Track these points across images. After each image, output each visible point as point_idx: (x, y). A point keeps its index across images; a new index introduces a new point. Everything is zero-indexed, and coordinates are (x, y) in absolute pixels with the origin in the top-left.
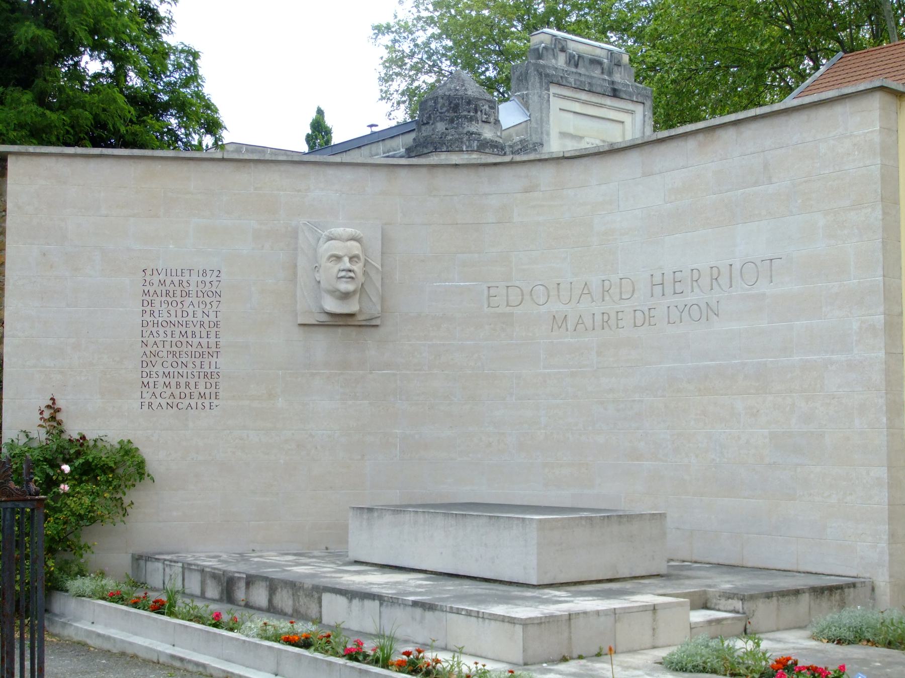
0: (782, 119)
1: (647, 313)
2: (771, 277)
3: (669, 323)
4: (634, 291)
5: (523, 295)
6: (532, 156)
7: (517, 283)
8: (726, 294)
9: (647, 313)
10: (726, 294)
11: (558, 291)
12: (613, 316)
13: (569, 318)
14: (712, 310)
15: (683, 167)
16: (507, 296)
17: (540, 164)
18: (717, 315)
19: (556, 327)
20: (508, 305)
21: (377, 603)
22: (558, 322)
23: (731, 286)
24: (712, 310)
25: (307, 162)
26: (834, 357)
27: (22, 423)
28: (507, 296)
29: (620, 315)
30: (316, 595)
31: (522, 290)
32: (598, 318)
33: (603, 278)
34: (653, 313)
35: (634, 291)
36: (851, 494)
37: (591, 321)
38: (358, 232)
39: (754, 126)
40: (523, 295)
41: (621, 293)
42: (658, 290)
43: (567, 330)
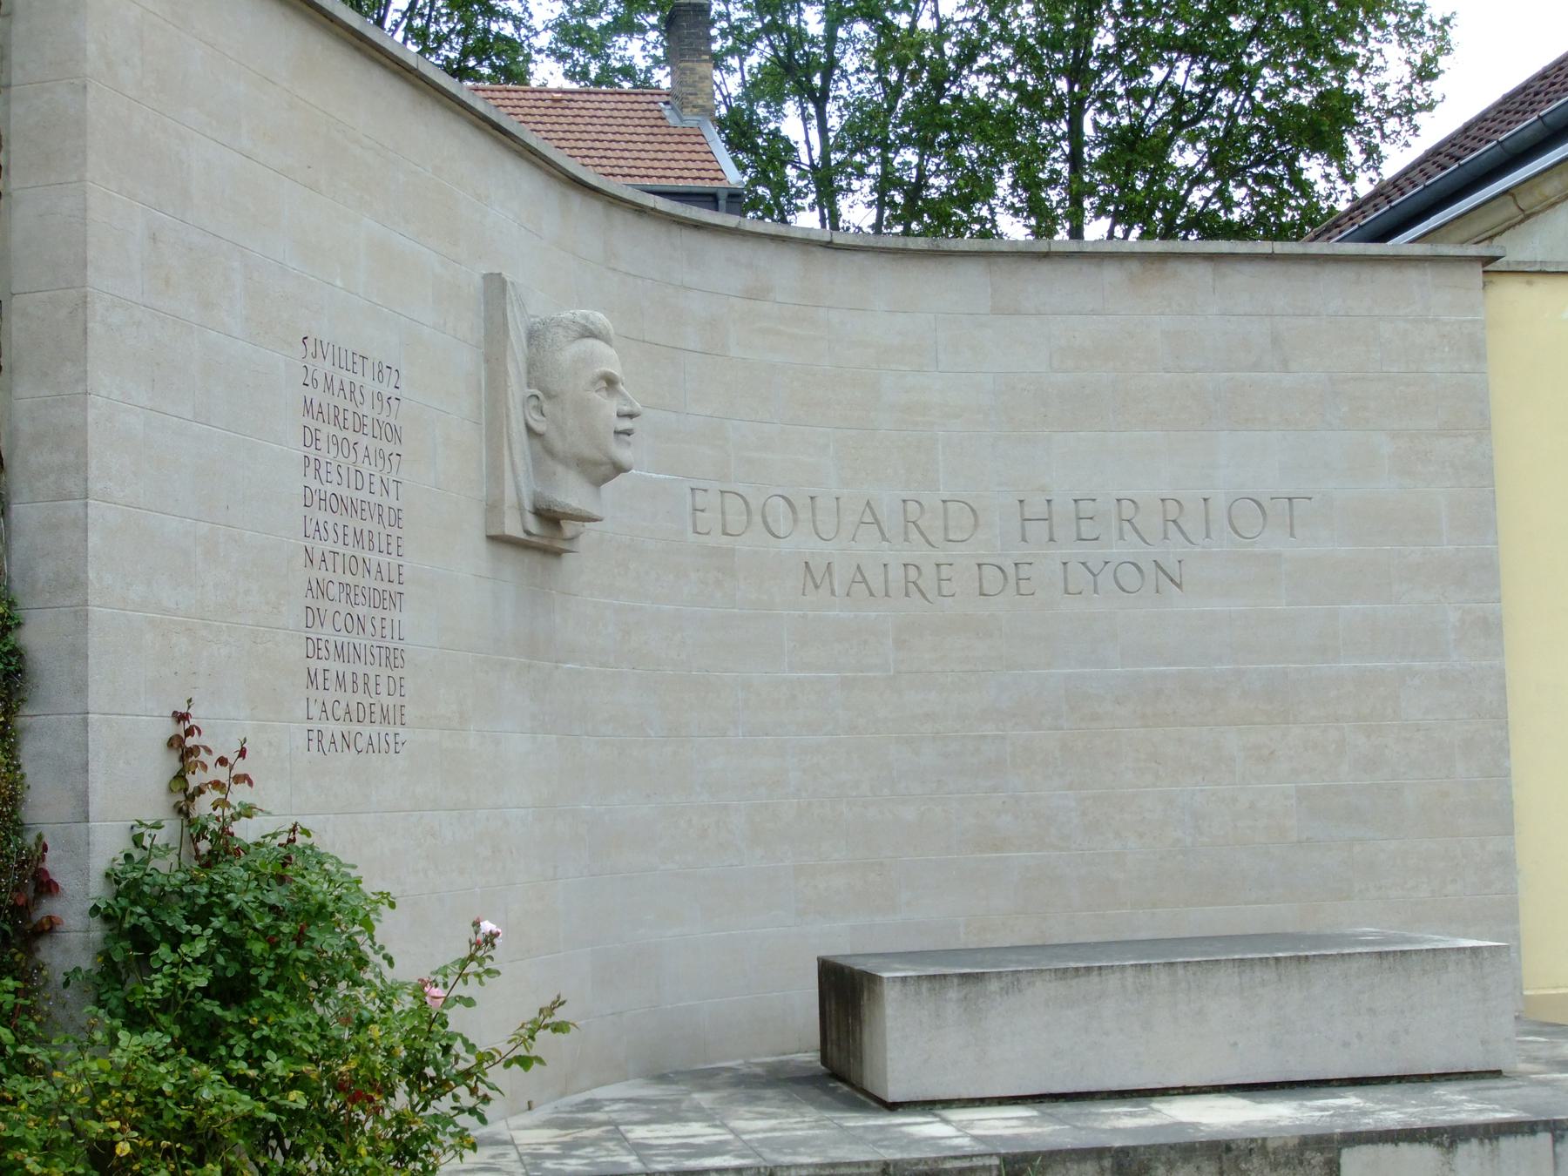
1: (1011, 571)
2: (1292, 527)
3: (1067, 592)
6: (769, 226)
7: (741, 488)
8: (1198, 549)
9: (1011, 571)
10: (1198, 549)
11: (814, 514)
12: (929, 570)
13: (835, 568)
15: (1093, 312)
18: (1179, 586)
19: (810, 585)
21: (1544, 1138)
22: (813, 575)
23: (1208, 536)
25: (534, 152)
26: (1418, 665)
27: (101, 808)
28: (723, 513)
30: (1318, 1158)
32: (896, 573)
33: (905, 495)
34: (1025, 571)
36: (1454, 881)
37: (882, 578)
39: (1248, 269)
41: (946, 528)
42: (1037, 530)
43: (833, 593)
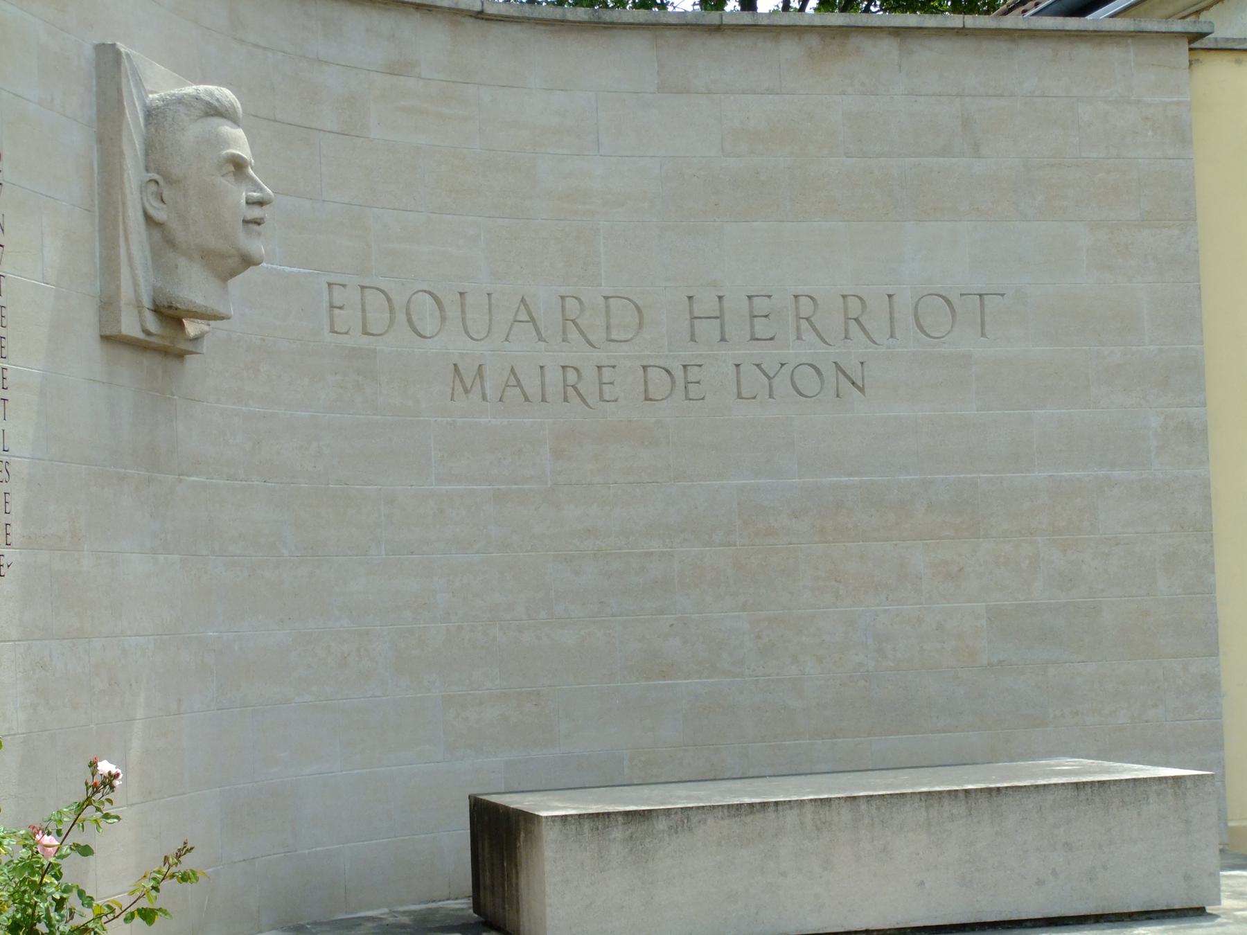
0: (1001, 46)
1: (679, 374)
3: (739, 396)
4: (641, 325)
5: (392, 310)
7: (382, 283)
9: (679, 374)
11: (463, 311)
12: (590, 374)
13: (487, 370)
14: (462, 380)
15: (770, 92)
16: (364, 310)
17: (417, 15)
18: (861, 390)
20: (366, 333)
24: (462, 380)
26: (1116, 473)
28: (364, 310)
29: (607, 374)
31: (389, 300)
32: (554, 377)
33: (563, 290)
35: (641, 325)
38: (238, 105)
39: (940, 45)
40: (392, 310)
41: (608, 328)
42: (707, 329)
43: (484, 398)
